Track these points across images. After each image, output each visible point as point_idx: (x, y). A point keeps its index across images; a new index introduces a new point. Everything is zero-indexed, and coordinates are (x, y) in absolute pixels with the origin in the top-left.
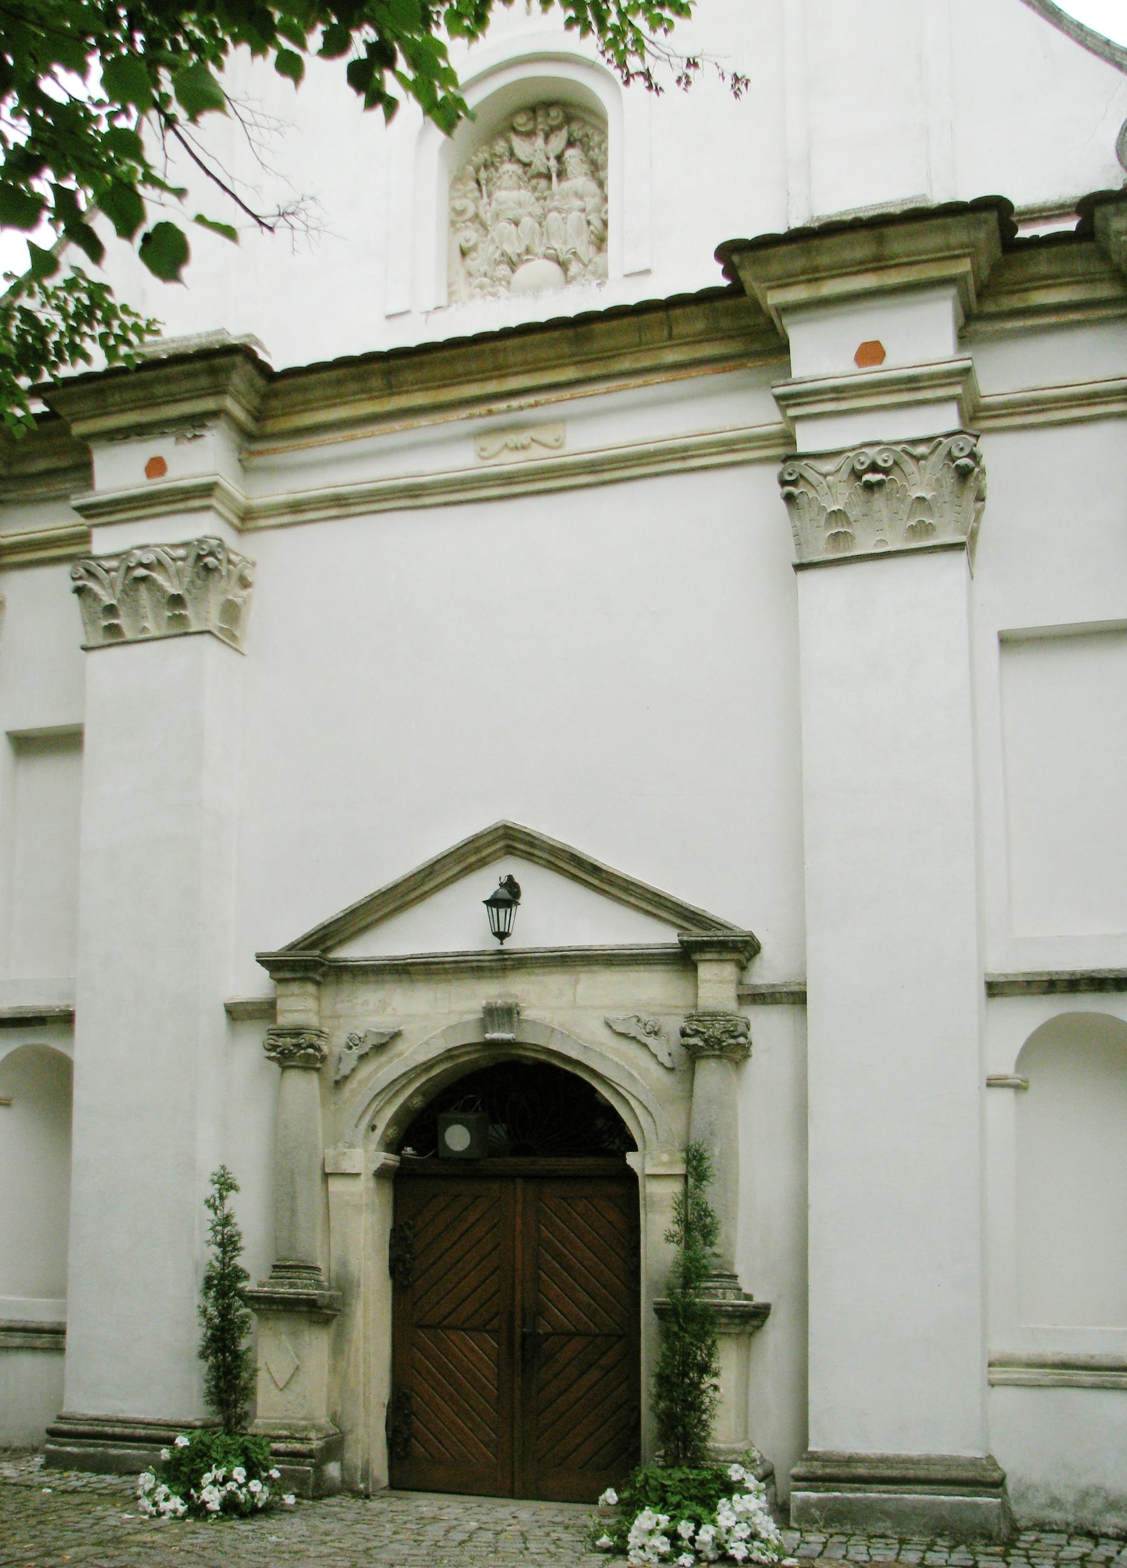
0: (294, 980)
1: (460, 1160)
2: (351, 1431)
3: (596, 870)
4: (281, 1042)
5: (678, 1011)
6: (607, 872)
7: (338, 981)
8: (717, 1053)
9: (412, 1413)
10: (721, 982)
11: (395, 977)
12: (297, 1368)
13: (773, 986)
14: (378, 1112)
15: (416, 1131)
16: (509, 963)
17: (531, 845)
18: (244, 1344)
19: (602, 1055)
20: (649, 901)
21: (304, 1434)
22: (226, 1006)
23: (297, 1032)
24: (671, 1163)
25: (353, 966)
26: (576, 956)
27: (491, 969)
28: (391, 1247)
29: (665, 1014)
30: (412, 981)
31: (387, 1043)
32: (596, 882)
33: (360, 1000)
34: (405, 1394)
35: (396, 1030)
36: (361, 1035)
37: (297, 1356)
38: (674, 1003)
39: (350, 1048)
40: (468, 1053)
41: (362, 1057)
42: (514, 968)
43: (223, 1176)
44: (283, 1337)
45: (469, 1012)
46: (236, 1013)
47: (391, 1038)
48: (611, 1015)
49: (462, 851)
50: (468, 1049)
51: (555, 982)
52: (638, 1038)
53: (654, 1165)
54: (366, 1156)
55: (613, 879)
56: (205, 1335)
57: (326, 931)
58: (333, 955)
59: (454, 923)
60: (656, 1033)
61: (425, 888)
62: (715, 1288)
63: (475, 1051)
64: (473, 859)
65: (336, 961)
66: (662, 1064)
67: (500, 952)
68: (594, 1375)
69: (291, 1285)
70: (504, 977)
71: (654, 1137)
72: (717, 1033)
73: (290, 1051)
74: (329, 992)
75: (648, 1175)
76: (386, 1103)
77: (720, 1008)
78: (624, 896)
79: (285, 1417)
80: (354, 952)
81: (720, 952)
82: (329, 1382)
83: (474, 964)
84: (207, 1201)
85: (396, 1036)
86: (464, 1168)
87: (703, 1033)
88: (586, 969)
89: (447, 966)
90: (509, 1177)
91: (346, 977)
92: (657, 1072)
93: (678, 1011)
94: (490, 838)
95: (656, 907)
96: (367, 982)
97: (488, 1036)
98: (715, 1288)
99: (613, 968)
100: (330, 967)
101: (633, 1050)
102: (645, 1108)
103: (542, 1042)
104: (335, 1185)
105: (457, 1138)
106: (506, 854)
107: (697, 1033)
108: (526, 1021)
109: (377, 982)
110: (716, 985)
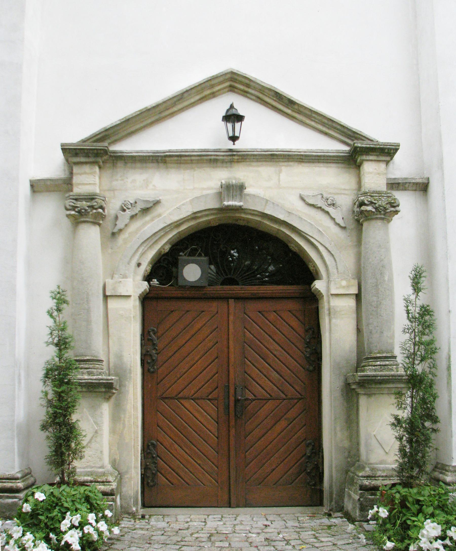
0: (86, 163)
1: (194, 287)
2: (127, 472)
3: (291, 103)
4: (79, 204)
5: (346, 192)
6: (298, 104)
7: (114, 165)
8: (383, 216)
9: (158, 456)
10: (378, 174)
11: (155, 165)
12: (96, 432)
13: (406, 179)
14: (143, 254)
15: (164, 269)
16: (236, 158)
17: (248, 86)
18: (74, 418)
19: (301, 218)
20: (324, 124)
21: (104, 479)
22: (31, 181)
23: (91, 198)
24: (348, 287)
25: (127, 156)
26: (280, 155)
27: (223, 162)
28: (142, 346)
29: (338, 194)
30: (167, 168)
31: (151, 207)
32: (289, 111)
33: (130, 180)
34: (153, 444)
35: (158, 199)
36: (132, 202)
37: (95, 423)
38: (343, 187)
39: (124, 210)
40: (206, 215)
41: (132, 217)
42: (238, 162)
43: (59, 293)
44: (85, 410)
45: (208, 189)
46: (37, 187)
47: (154, 204)
48: (305, 193)
49: (203, 86)
50: (207, 213)
51: (266, 171)
52: (323, 207)
53: (337, 288)
54: (134, 285)
55: (301, 109)
56: (48, 412)
57: (107, 133)
58: (113, 148)
59: (200, 129)
60: (333, 205)
61: (175, 109)
62: (391, 365)
63: (212, 214)
64: (208, 92)
65: (114, 152)
66: (338, 225)
67: (231, 150)
68: (283, 423)
69: (89, 373)
70: (231, 167)
71: (335, 271)
72: (384, 204)
73: (86, 210)
74: (107, 173)
75: (332, 295)
76: (148, 249)
77: (378, 189)
78: (308, 121)
79: (87, 467)
80: (126, 147)
81: (377, 156)
82: (110, 440)
83: (212, 157)
84: (48, 312)
85: (157, 203)
86: (195, 293)
87: (375, 203)
88: (286, 164)
89: (193, 158)
90: (226, 299)
91: (120, 164)
92: (335, 230)
93: (346, 192)
94: (221, 79)
95: (328, 128)
96: (135, 168)
97: (226, 203)
98: (391, 365)
99: (303, 164)
100: (111, 156)
101: (319, 215)
102: (329, 251)
103: (259, 208)
104: (112, 304)
105: (192, 273)
106: (228, 91)
107: (371, 203)
108: (248, 195)
109: (142, 168)
110: (374, 175)
